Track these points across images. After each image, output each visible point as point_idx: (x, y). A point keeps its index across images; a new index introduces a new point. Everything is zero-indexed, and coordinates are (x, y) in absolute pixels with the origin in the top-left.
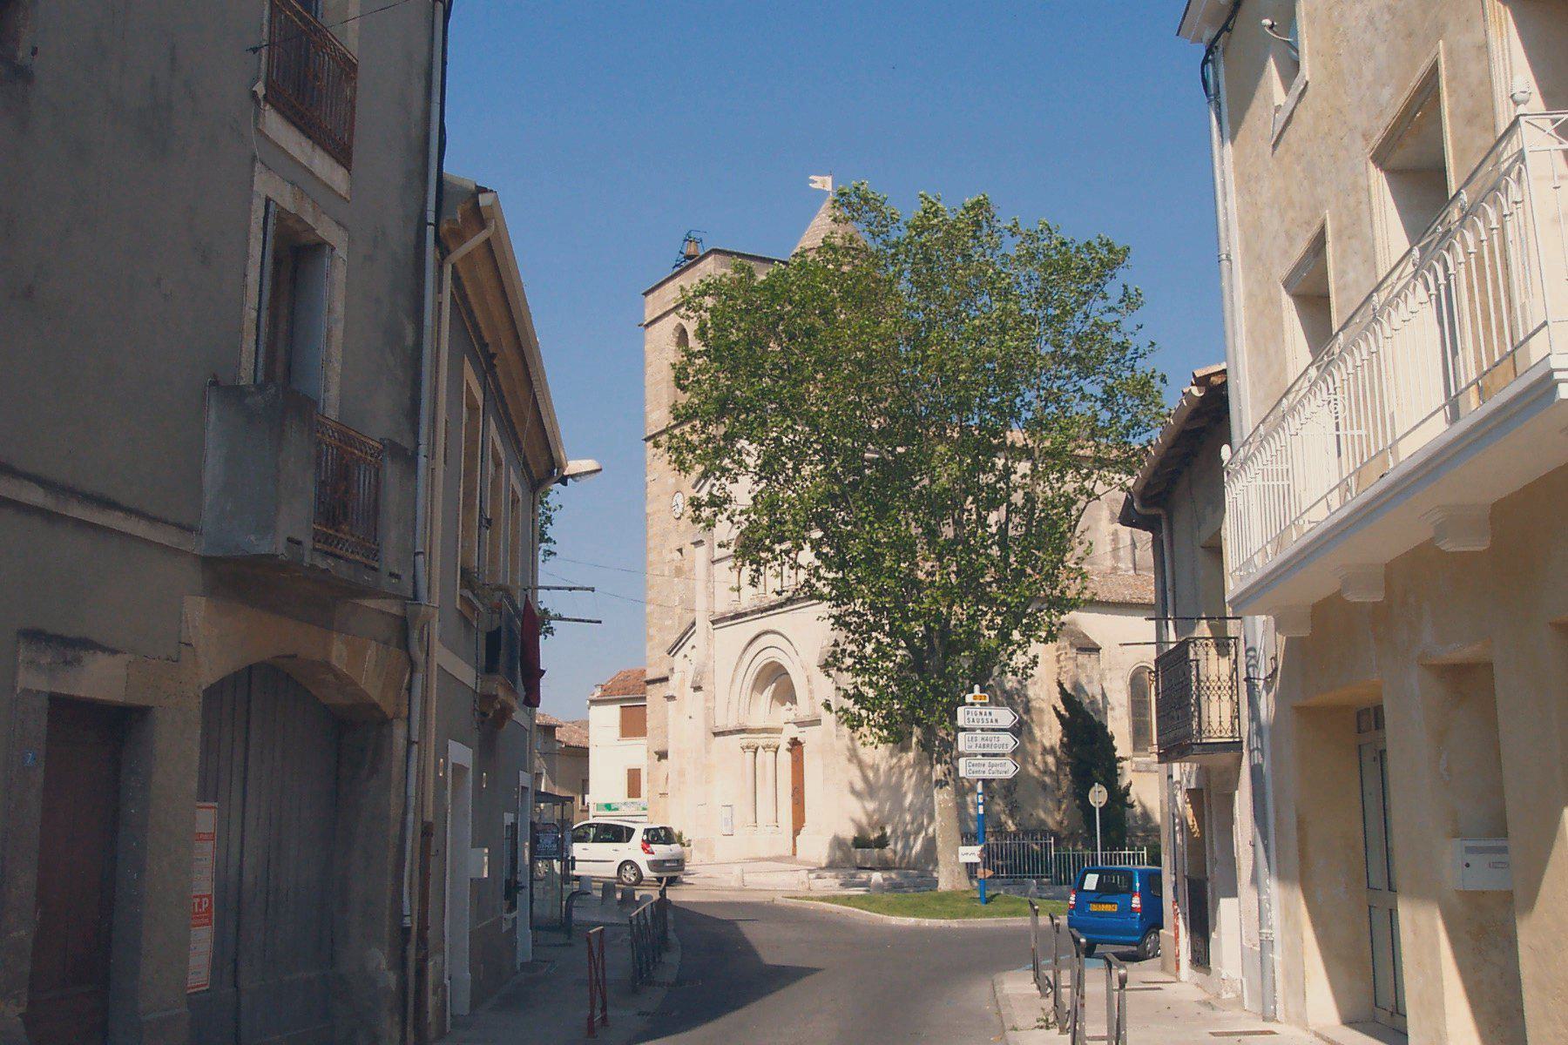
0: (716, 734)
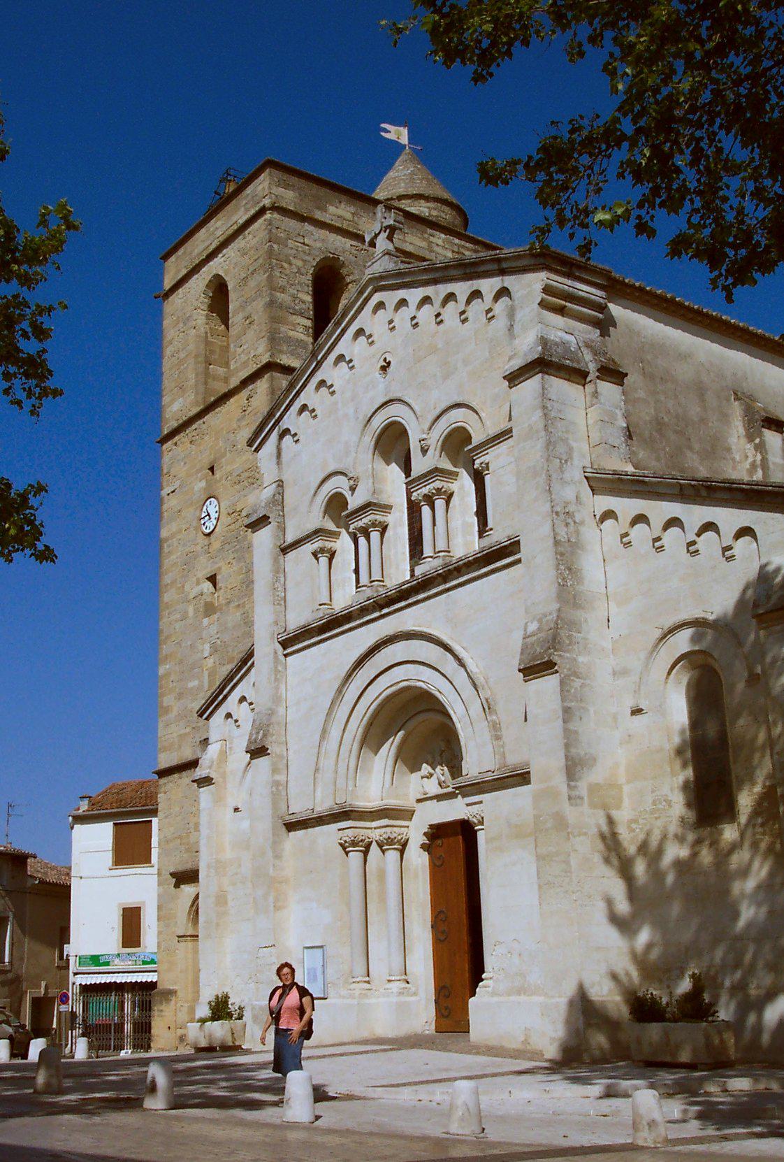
0: (291, 826)
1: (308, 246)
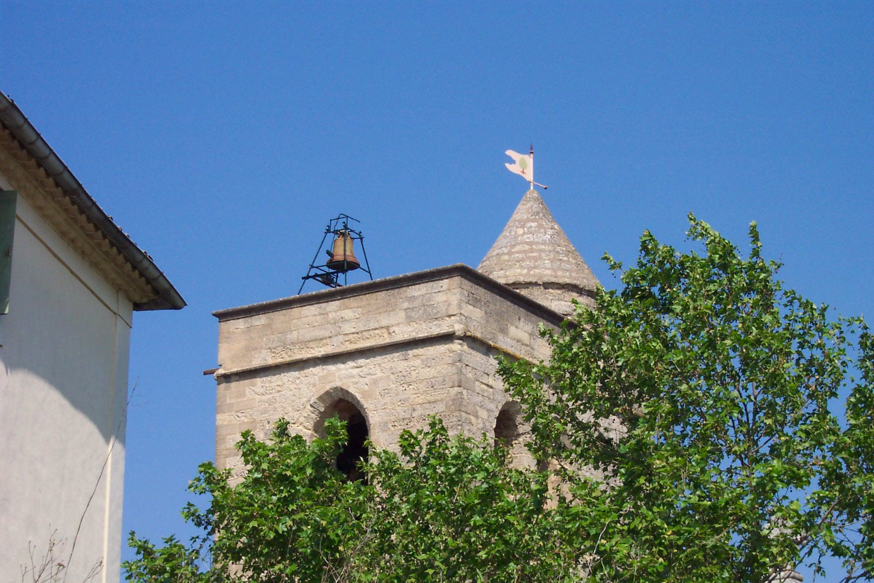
1: (492, 387)
